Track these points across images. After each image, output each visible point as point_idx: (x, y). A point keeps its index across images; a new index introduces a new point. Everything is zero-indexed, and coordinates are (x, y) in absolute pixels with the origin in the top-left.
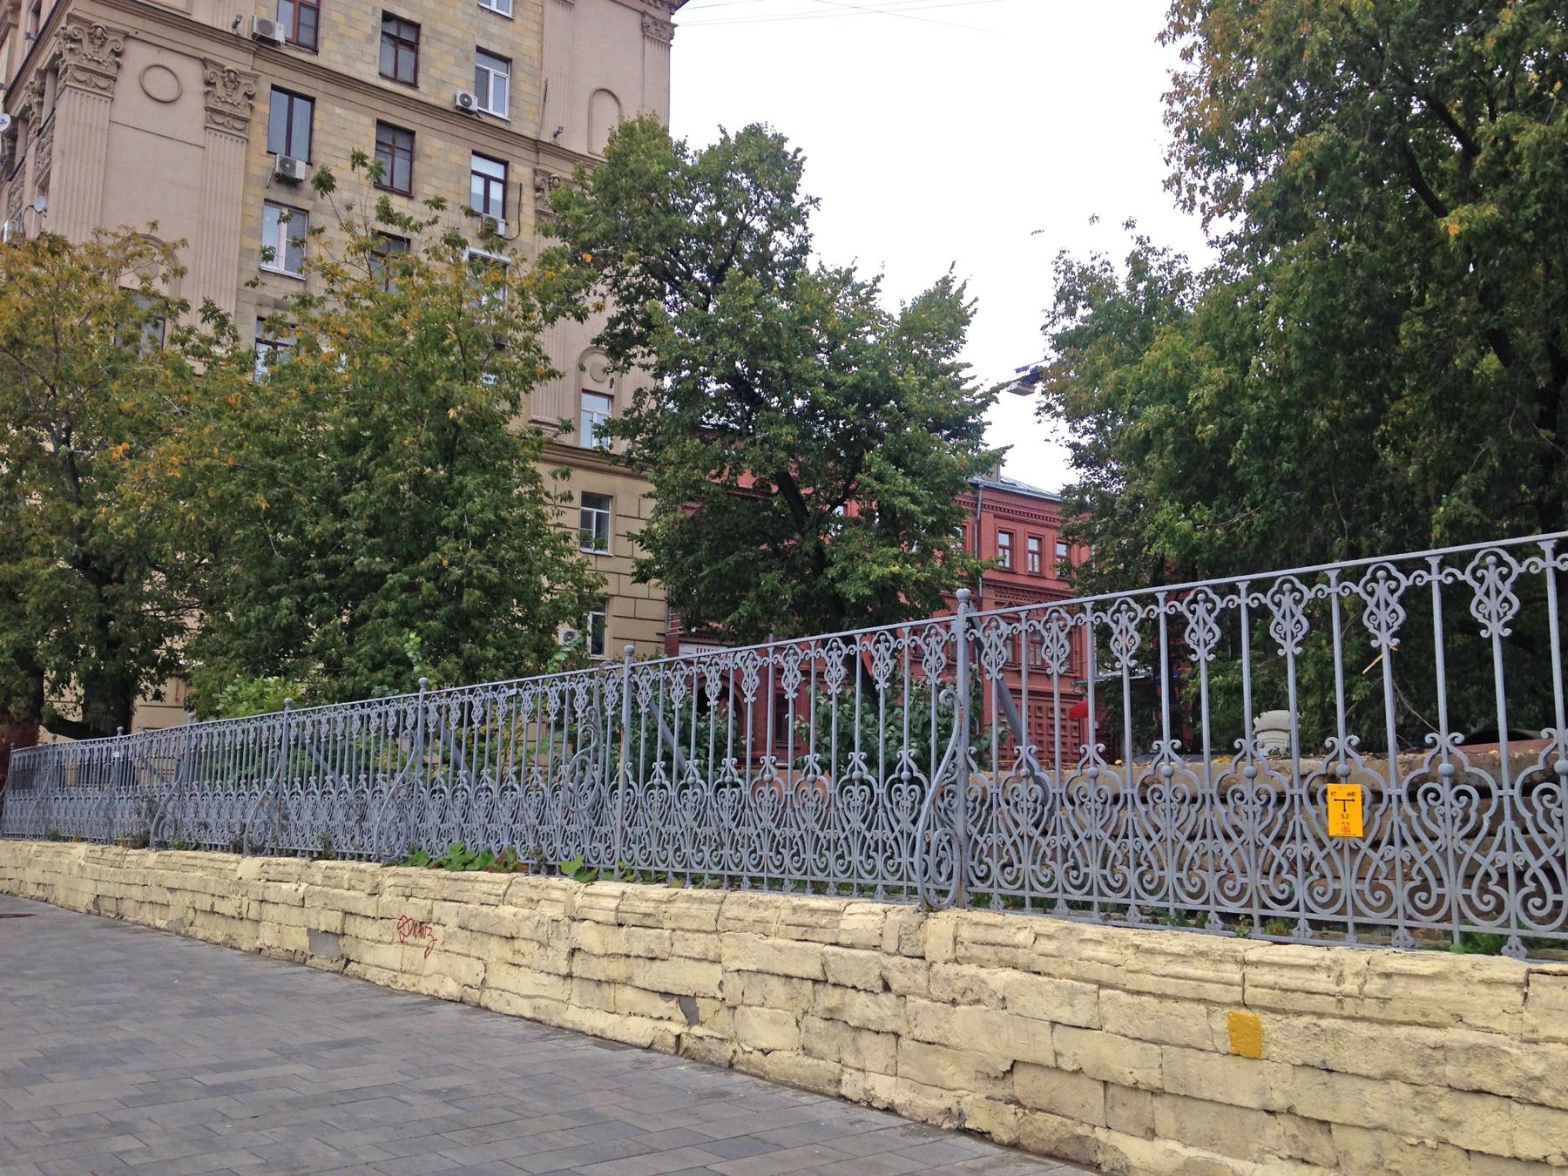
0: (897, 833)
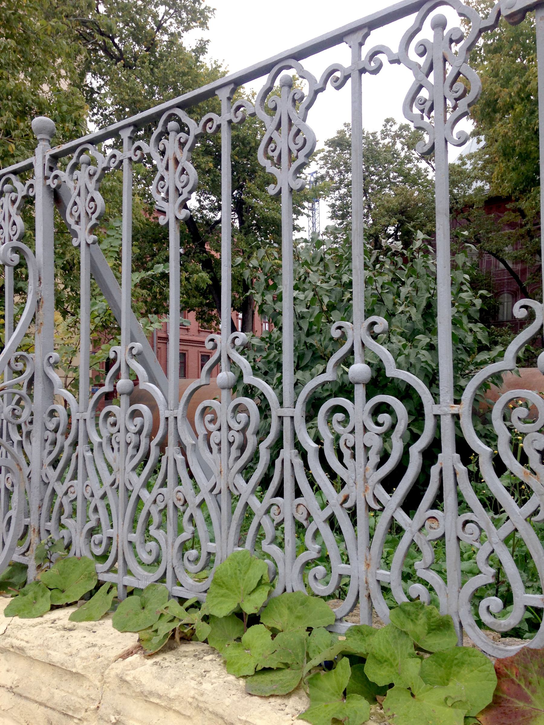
0: (204, 494)
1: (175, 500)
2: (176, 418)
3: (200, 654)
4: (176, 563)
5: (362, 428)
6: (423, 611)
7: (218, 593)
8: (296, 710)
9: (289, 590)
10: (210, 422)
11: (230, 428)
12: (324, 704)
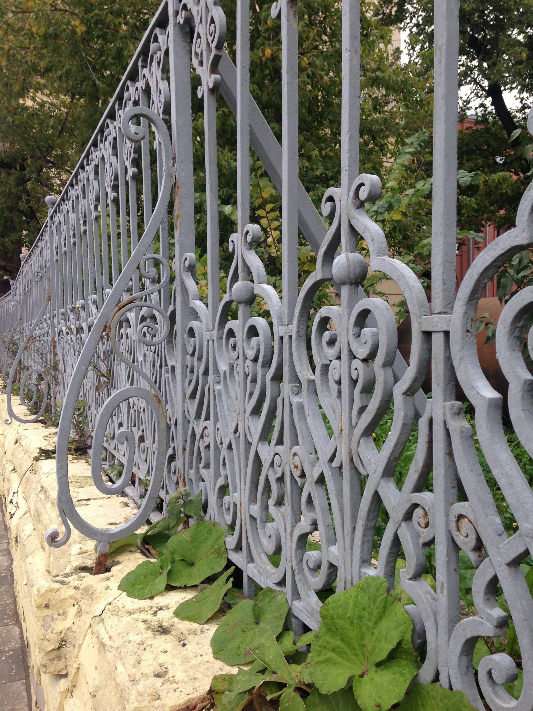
1: (292, 466)
2: (290, 337)
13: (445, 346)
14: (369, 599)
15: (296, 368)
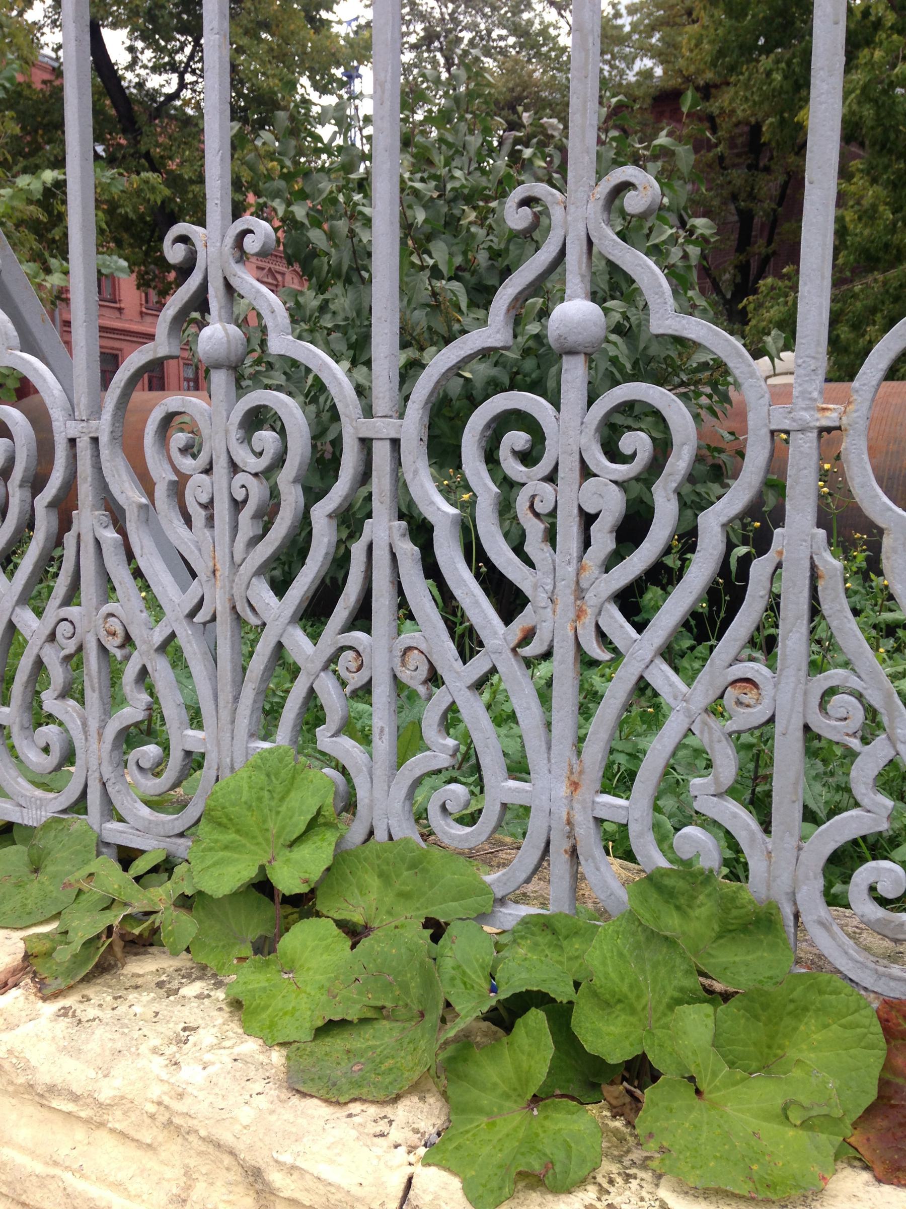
2: (95, 440)
3: (171, 979)
4: (107, 772)
5: (577, 465)
6: (709, 889)
7: (216, 841)
8: (416, 1131)
9: (380, 835)
10: (184, 451)
11: (234, 468)
12: (484, 1120)
13: (393, 457)
14: (268, 775)
15: (111, 487)
